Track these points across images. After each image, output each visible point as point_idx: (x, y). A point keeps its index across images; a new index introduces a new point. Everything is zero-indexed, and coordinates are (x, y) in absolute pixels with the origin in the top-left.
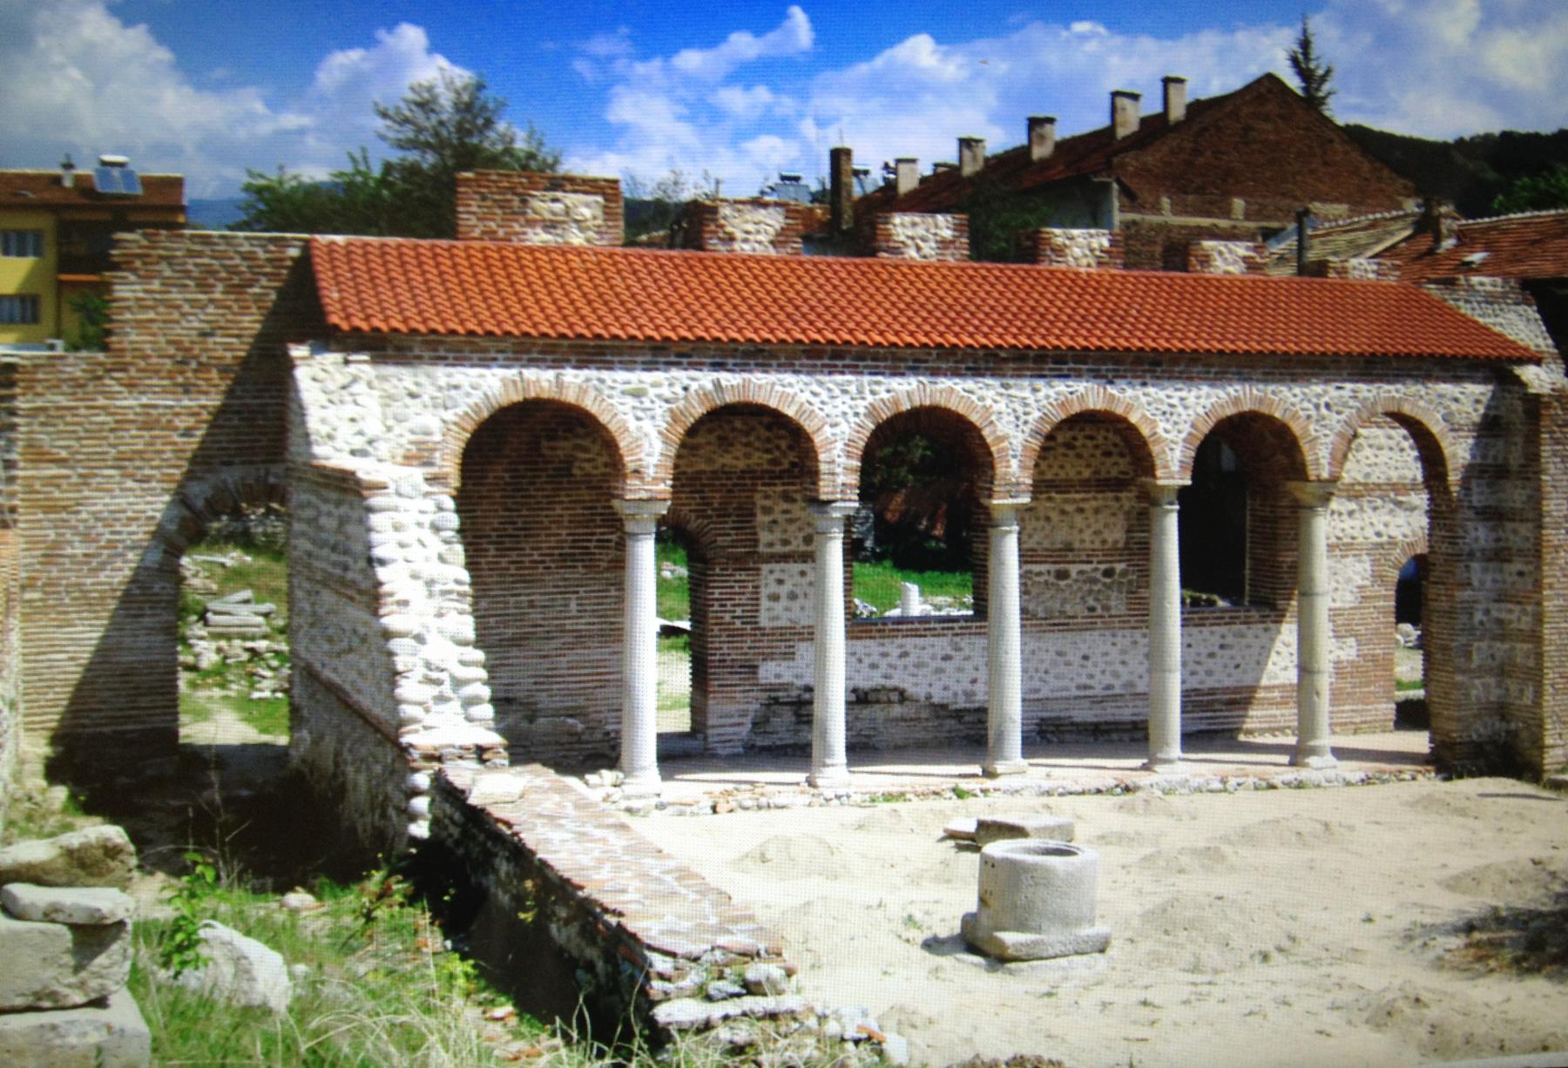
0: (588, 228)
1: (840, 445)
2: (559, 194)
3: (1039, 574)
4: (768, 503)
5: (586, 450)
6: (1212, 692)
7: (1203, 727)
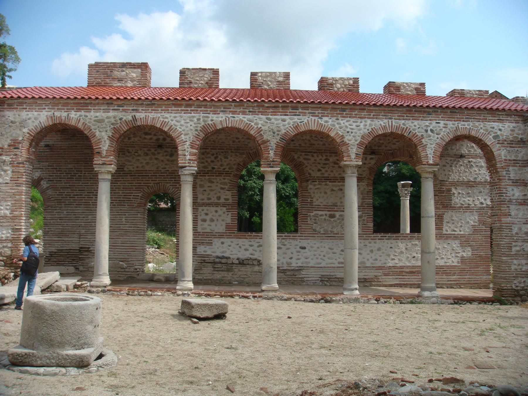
0: (135, 81)
1: (188, 143)
2: (124, 69)
3: (321, 215)
4: (202, 183)
5: (130, 161)
6: (402, 267)
7: (398, 283)
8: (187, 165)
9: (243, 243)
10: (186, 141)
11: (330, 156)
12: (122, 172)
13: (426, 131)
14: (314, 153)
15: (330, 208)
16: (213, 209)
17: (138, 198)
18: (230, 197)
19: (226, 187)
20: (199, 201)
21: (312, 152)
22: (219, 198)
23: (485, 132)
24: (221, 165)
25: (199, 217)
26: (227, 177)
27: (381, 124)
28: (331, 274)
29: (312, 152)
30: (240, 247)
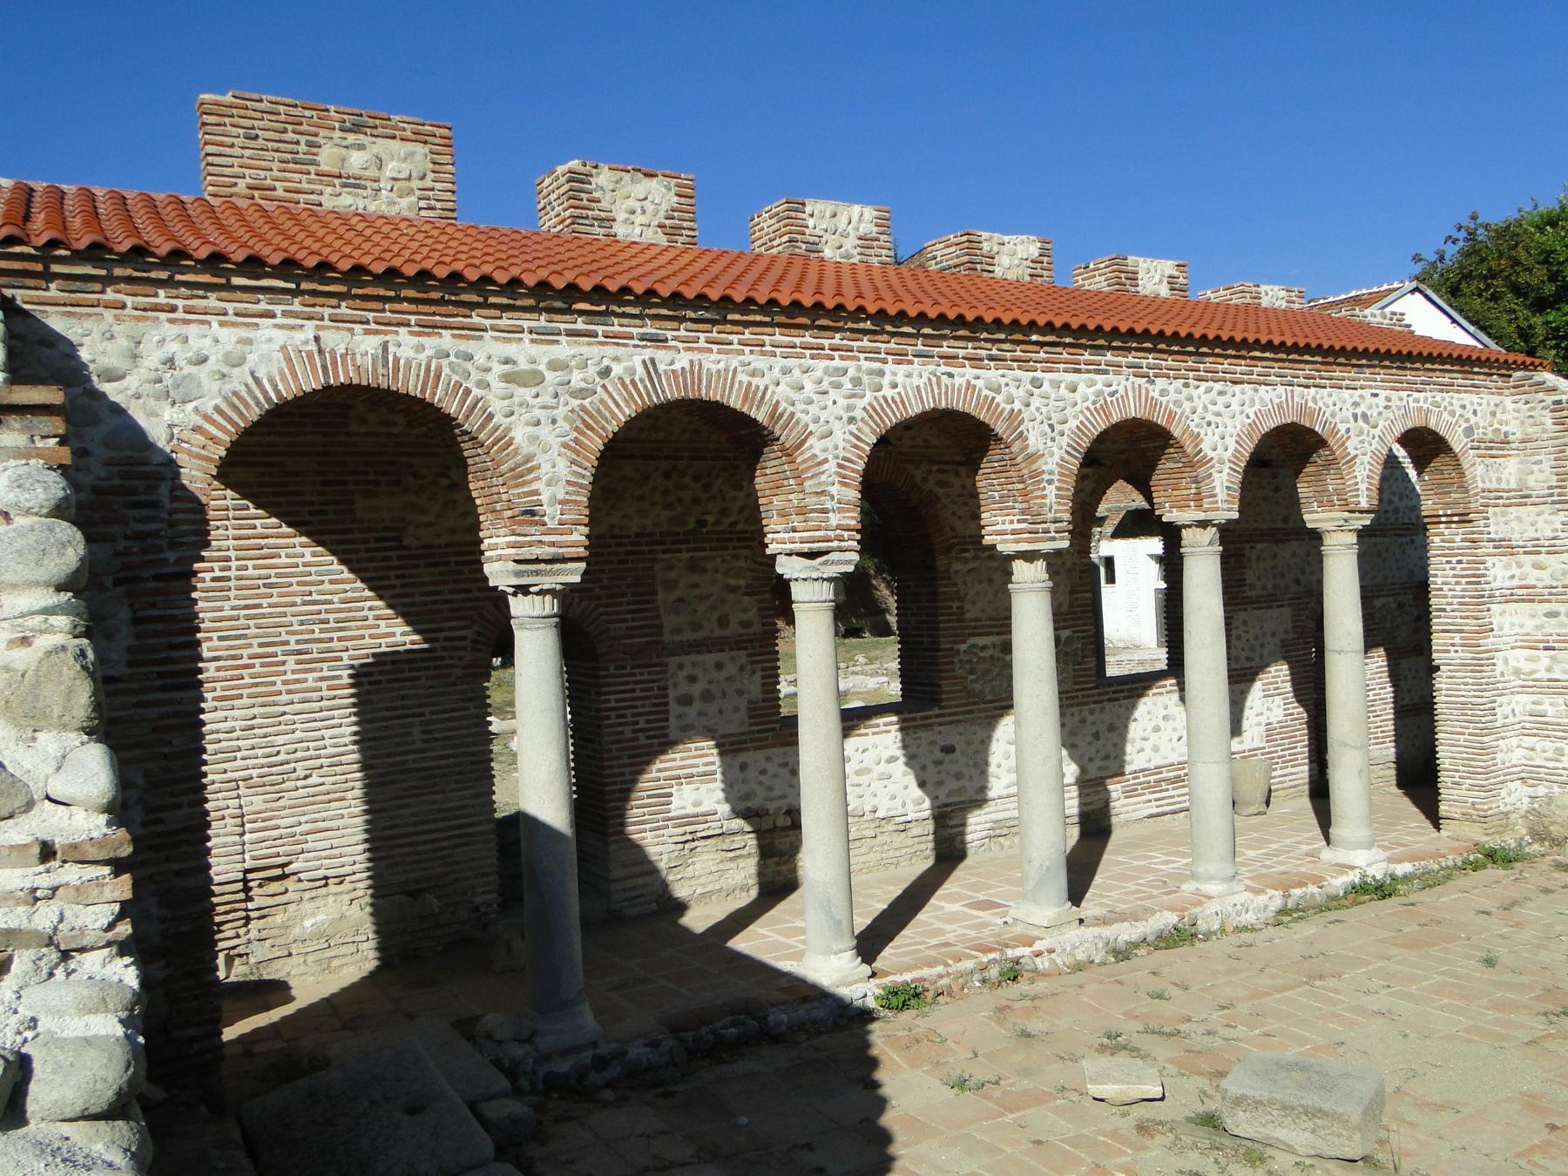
1: (831, 466)
3: (984, 648)
8: (835, 544)
10: (826, 461)
12: (394, 554)
16: (711, 658)
17: (463, 648)
18: (752, 615)
19: (742, 583)
22: (723, 621)
24: (724, 512)
26: (745, 552)
27: (914, 381)
29: (954, 463)
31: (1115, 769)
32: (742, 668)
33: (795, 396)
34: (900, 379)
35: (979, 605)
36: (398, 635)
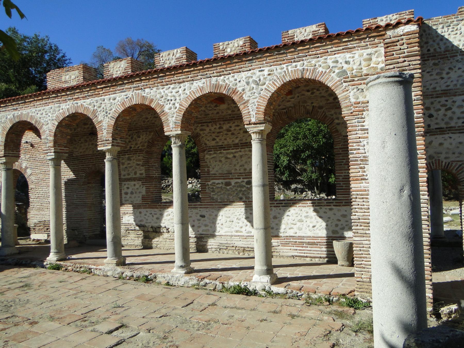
1: (48, 132)
5: (76, 148)
9: (155, 213)
11: (223, 124)
13: (248, 83)
14: (209, 122)
15: (225, 176)
16: (133, 183)
18: (143, 172)
20: (122, 177)
21: (207, 122)
22: (135, 173)
23: (324, 71)
24: (136, 144)
25: (123, 190)
28: (229, 242)
29: (207, 122)
30: (153, 216)
31: (276, 234)
32: (140, 186)
33: (41, 116)
34: (63, 107)
35: (215, 169)
36: (71, 175)
